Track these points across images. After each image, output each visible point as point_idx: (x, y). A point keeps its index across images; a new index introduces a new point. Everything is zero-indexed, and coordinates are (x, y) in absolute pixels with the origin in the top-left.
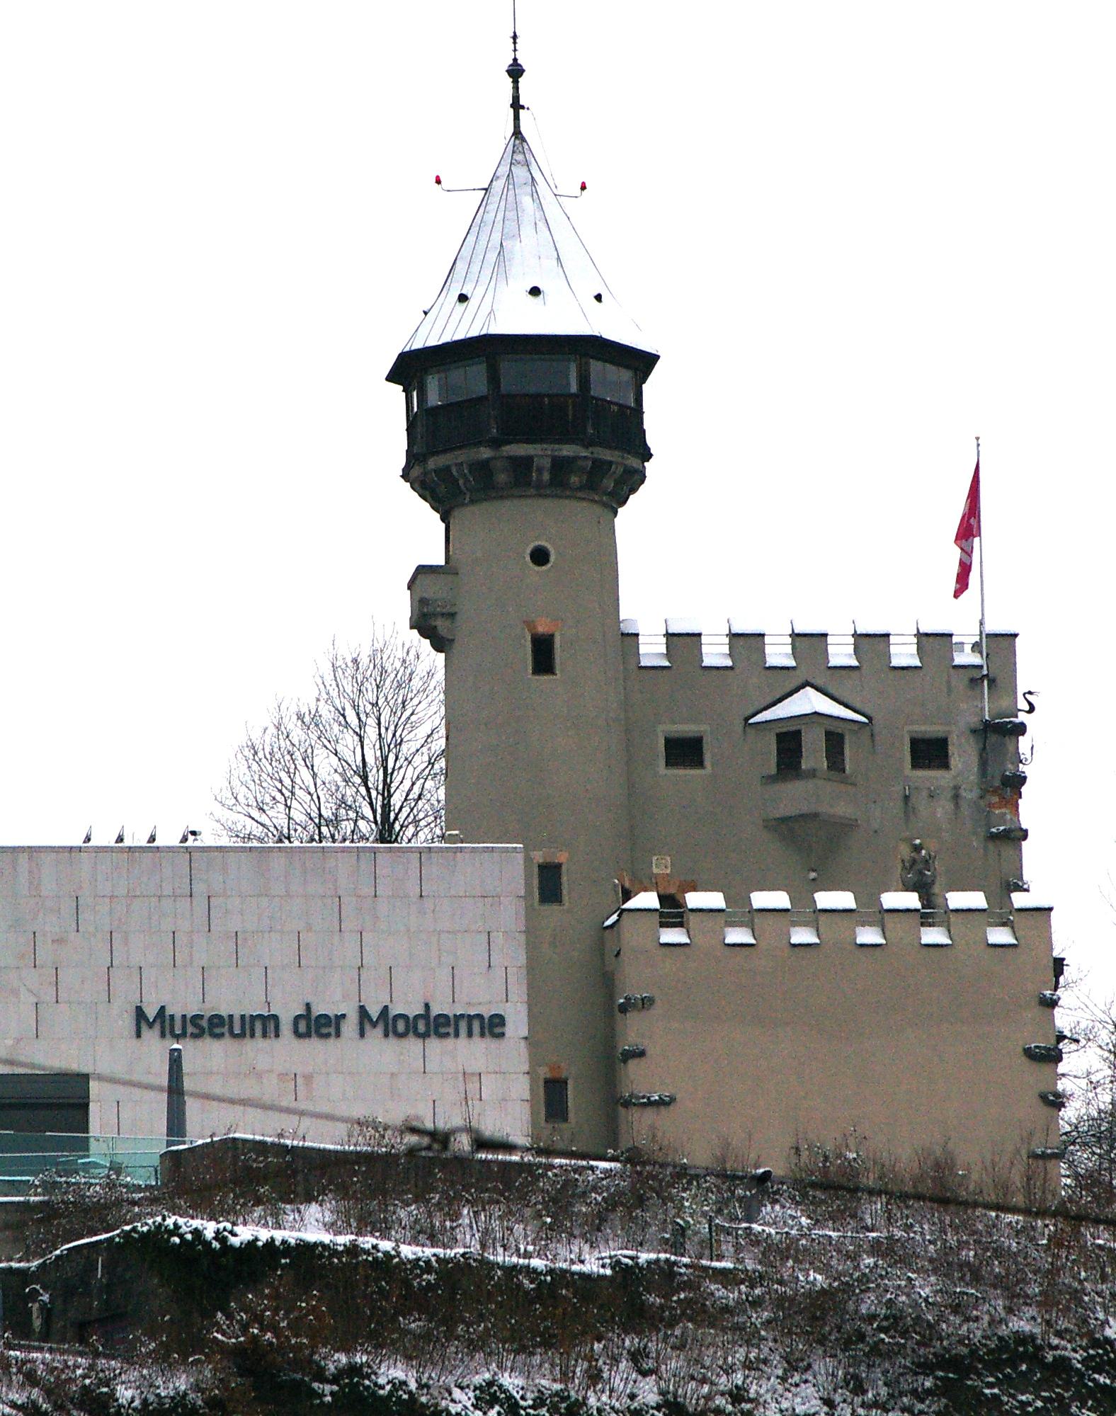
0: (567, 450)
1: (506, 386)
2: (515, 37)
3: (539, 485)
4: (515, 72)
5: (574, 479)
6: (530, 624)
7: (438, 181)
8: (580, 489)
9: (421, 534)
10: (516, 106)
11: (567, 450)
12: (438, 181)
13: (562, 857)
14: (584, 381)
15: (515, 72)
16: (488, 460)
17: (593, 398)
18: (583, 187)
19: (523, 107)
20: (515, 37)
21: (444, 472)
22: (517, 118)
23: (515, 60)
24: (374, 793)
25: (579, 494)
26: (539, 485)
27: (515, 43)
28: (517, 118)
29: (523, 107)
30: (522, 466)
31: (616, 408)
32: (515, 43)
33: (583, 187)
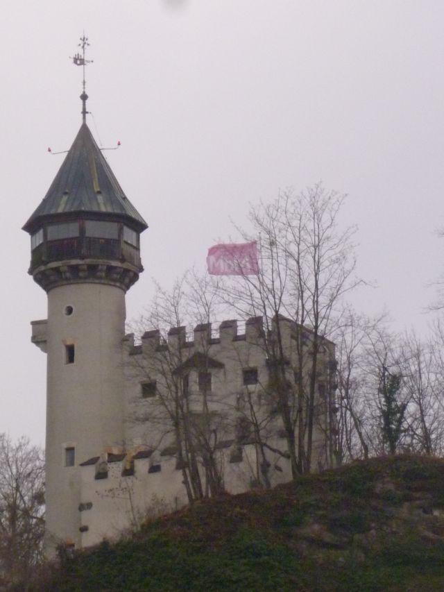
0: (74, 262)
1: (88, 234)
2: (84, 83)
3: (67, 279)
4: (84, 97)
5: (81, 274)
6: (64, 341)
7: (50, 150)
8: (85, 278)
9: (37, 302)
10: (84, 112)
11: (74, 262)
12: (50, 150)
13: (73, 444)
14: (82, 231)
15: (84, 97)
16: (44, 270)
17: (87, 238)
18: (119, 144)
19: (87, 113)
20: (84, 83)
21: (43, 273)
22: (84, 118)
23: (84, 92)
24: (179, 391)
25: (87, 281)
26: (67, 279)
27: (84, 85)
28: (84, 118)
29: (87, 113)
30: (75, 269)
31: (103, 241)
32: (84, 85)
33: (119, 144)
